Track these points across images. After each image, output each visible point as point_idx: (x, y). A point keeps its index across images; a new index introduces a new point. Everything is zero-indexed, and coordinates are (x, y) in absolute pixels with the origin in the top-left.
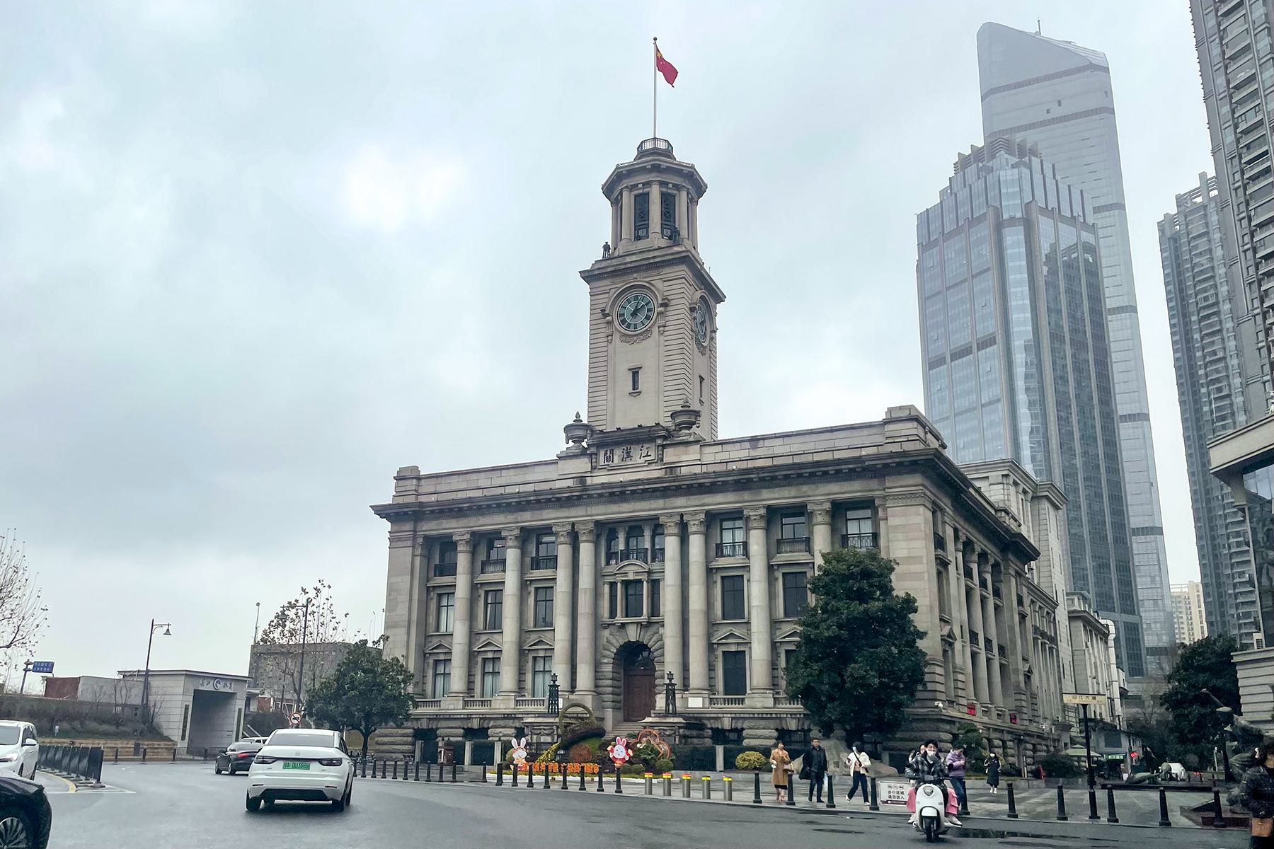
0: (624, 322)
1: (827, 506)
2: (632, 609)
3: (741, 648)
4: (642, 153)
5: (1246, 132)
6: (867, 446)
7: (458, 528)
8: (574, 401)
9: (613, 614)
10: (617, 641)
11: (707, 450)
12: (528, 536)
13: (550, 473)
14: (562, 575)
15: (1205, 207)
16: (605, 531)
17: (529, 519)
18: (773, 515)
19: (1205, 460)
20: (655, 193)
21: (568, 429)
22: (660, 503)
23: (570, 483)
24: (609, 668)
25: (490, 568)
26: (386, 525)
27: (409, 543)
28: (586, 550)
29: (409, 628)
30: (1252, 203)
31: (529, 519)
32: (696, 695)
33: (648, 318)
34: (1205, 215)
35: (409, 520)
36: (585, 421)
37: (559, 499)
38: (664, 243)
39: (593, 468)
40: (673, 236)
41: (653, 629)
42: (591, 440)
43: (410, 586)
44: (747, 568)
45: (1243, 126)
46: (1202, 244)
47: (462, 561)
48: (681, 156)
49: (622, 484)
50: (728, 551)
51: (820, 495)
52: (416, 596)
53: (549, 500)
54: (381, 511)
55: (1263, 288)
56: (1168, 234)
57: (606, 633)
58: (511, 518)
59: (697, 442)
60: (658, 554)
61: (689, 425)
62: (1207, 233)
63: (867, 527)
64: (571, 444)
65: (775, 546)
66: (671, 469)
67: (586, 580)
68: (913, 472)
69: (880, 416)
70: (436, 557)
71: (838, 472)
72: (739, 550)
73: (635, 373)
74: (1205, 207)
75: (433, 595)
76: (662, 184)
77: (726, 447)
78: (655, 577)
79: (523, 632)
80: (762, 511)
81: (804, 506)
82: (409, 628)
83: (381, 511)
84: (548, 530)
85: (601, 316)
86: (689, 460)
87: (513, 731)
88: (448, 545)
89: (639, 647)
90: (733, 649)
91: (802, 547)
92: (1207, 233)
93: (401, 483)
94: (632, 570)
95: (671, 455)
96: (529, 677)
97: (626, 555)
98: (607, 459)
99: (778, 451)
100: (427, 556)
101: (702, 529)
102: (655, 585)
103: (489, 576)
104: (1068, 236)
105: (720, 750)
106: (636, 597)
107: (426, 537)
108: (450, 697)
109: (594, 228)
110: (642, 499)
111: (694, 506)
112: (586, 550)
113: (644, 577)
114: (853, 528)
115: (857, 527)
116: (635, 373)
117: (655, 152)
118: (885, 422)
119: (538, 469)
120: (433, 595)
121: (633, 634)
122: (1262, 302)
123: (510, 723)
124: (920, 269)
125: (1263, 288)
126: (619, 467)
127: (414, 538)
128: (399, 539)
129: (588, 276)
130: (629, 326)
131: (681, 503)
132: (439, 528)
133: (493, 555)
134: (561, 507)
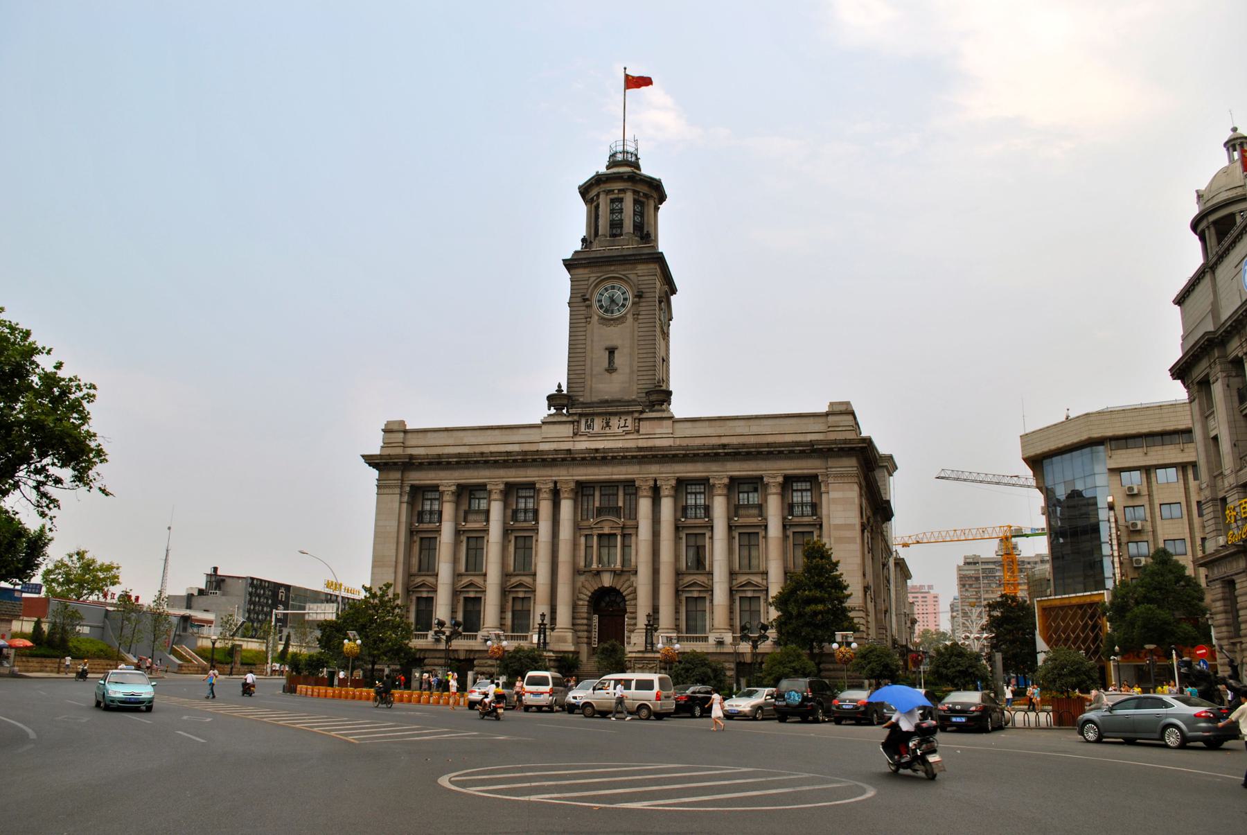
3: (430, 595)
4: (613, 163)
6: (814, 433)
7: (448, 481)
8: (557, 376)
10: (591, 586)
11: (677, 425)
12: (510, 490)
13: (534, 435)
16: (582, 490)
18: (735, 484)
20: (624, 199)
26: (375, 473)
27: (398, 491)
28: (566, 506)
35: (397, 470)
37: (544, 460)
39: (575, 434)
41: (624, 578)
44: (486, 531)
48: (647, 170)
50: (427, 518)
51: (773, 471)
52: (402, 539)
54: (371, 460)
57: (582, 578)
60: (633, 514)
64: (553, 411)
65: (734, 510)
67: (566, 532)
69: (825, 409)
72: (808, 510)
73: (611, 351)
75: (464, 538)
76: (635, 192)
79: (505, 575)
81: (707, 479)
83: (371, 460)
86: (657, 436)
89: (612, 591)
91: (755, 512)
95: (645, 427)
98: (588, 427)
107: (412, 486)
109: (571, 227)
110: (621, 464)
111: (667, 474)
112: (566, 506)
113: (618, 532)
116: (611, 351)
117: (625, 163)
118: (827, 414)
119: (522, 431)
121: (607, 580)
126: (598, 435)
127: (402, 487)
129: (569, 264)
131: (654, 470)
134: (544, 466)
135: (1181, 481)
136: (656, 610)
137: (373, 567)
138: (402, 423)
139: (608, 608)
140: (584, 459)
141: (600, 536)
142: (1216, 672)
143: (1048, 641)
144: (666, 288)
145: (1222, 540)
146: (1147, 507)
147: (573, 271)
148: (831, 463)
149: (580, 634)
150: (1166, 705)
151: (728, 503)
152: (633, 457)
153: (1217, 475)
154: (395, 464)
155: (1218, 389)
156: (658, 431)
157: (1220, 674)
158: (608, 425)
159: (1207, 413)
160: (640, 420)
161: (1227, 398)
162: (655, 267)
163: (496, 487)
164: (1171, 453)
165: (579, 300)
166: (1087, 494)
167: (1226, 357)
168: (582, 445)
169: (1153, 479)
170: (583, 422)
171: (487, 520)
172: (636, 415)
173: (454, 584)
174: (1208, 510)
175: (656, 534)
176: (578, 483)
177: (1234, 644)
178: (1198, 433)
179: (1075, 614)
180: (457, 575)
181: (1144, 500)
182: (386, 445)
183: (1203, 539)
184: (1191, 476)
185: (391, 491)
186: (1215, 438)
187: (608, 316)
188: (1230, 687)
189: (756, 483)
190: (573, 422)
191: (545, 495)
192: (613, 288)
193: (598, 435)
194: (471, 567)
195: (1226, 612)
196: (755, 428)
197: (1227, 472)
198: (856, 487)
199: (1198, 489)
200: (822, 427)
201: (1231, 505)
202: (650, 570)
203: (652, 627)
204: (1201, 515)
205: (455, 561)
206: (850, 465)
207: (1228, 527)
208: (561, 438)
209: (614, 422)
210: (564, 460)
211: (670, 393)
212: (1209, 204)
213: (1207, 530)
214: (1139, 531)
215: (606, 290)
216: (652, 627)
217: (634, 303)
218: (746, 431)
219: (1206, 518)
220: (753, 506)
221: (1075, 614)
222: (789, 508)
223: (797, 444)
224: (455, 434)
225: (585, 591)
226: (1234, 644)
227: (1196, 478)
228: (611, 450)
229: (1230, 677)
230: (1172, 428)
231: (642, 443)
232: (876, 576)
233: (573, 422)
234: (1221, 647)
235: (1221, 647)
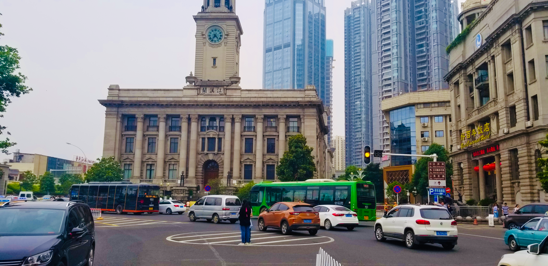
1: (285, 117)
2: (211, 148)
8: (190, 69)
9: (203, 149)
10: (205, 159)
14: (184, 133)
16: (201, 118)
17: (170, 111)
18: (267, 118)
19: (288, 104)
21: (187, 78)
24: (201, 169)
25: (150, 129)
26: (104, 108)
27: (115, 116)
28: (194, 125)
29: (115, 151)
31: (170, 111)
33: (209, 36)
36: (194, 76)
37: (184, 105)
38: (226, 10)
39: (198, 94)
40: (230, 8)
41: (219, 156)
42: (196, 82)
43: (116, 133)
49: (210, 102)
51: (282, 113)
54: (103, 103)
56: (347, 15)
57: (200, 156)
60: (222, 129)
63: (296, 124)
64: (188, 84)
65: (265, 129)
66: (230, 97)
68: (313, 108)
70: (128, 123)
72: (296, 130)
73: (215, 59)
77: (250, 92)
78: (220, 136)
82: (115, 151)
83: (103, 103)
84: (178, 116)
85: (200, 35)
86: (235, 96)
88: (132, 118)
89: (213, 161)
90: (248, 163)
93: (111, 91)
94: (212, 134)
95: (229, 93)
96: (167, 172)
97: (209, 128)
98: (204, 91)
99: (269, 96)
100: (122, 122)
101: (240, 121)
102: (220, 139)
103: (151, 132)
104: (317, 10)
106: (212, 144)
107: (123, 115)
108: (135, 179)
110: (218, 108)
111: (238, 113)
112: (194, 125)
113: (216, 137)
114: (291, 124)
115: (293, 124)
116: (215, 59)
120: (124, 138)
121: (211, 157)
124: (265, 12)
126: (208, 95)
127: (117, 115)
128: (110, 114)
131: (232, 111)
132: (127, 112)
133: (152, 124)
135: (444, 122)
136: (231, 169)
137: (104, 150)
138: (117, 86)
139: (210, 170)
141: (208, 138)
142: (453, 198)
143: (388, 183)
144: (238, 32)
145: (459, 147)
146: (430, 132)
147: (198, 22)
148: (306, 110)
149: (199, 180)
152: (223, 105)
153: (459, 121)
154: (115, 104)
155: (462, 86)
156: (234, 94)
157: (455, 199)
158: (213, 91)
159: (457, 96)
160: (227, 89)
161: (465, 91)
162: (234, 23)
163: (162, 116)
164: (441, 111)
165: (200, 34)
166: (407, 126)
167: (466, 73)
168: (201, 99)
169: (433, 121)
171: (158, 131)
172: (225, 87)
174: (454, 135)
175: (232, 138)
176: (199, 116)
177: (461, 188)
178: (452, 103)
179: (399, 174)
181: (429, 129)
183: (452, 146)
184: (448, 120)
185: (112, 117)
186: (459, 106)
188: (459, 205)
190: (197, 89)
191: (184, 120)
192: (216, 30)
193: (208, 95)
194: (150, 150)
195: (458, 175)
196: (276, 94)
197: (462, 120)
198: (315, 120)
199: (452, 125)
200: (303, 95)
201: (463, 133)
202: (229, 160)
203: (230, 177)
204: (451, 136)
205: (143, 148)
206: (313, 111)
207: (461, 142)
208: (191, 95)
209: (215, 90)
211: (239, 78)
212: (466, 9)
213: (453, 142)
214: (426, 142)
216: (230, 177)
218: (271, 96)
219: (453, 138)
220: (273, 127)
221: (399, 174)
222: (288, 129)
223: (293, 102)
225: (200, 163)
226: (461, 188)
227: (450, 121)
228: (215, 102)
229: (459, 200)
230: (442, 100)
231: (226, 99)
232: (321, 157)
233: (197, 89)
234: (456, 189)
235: (456, 189)
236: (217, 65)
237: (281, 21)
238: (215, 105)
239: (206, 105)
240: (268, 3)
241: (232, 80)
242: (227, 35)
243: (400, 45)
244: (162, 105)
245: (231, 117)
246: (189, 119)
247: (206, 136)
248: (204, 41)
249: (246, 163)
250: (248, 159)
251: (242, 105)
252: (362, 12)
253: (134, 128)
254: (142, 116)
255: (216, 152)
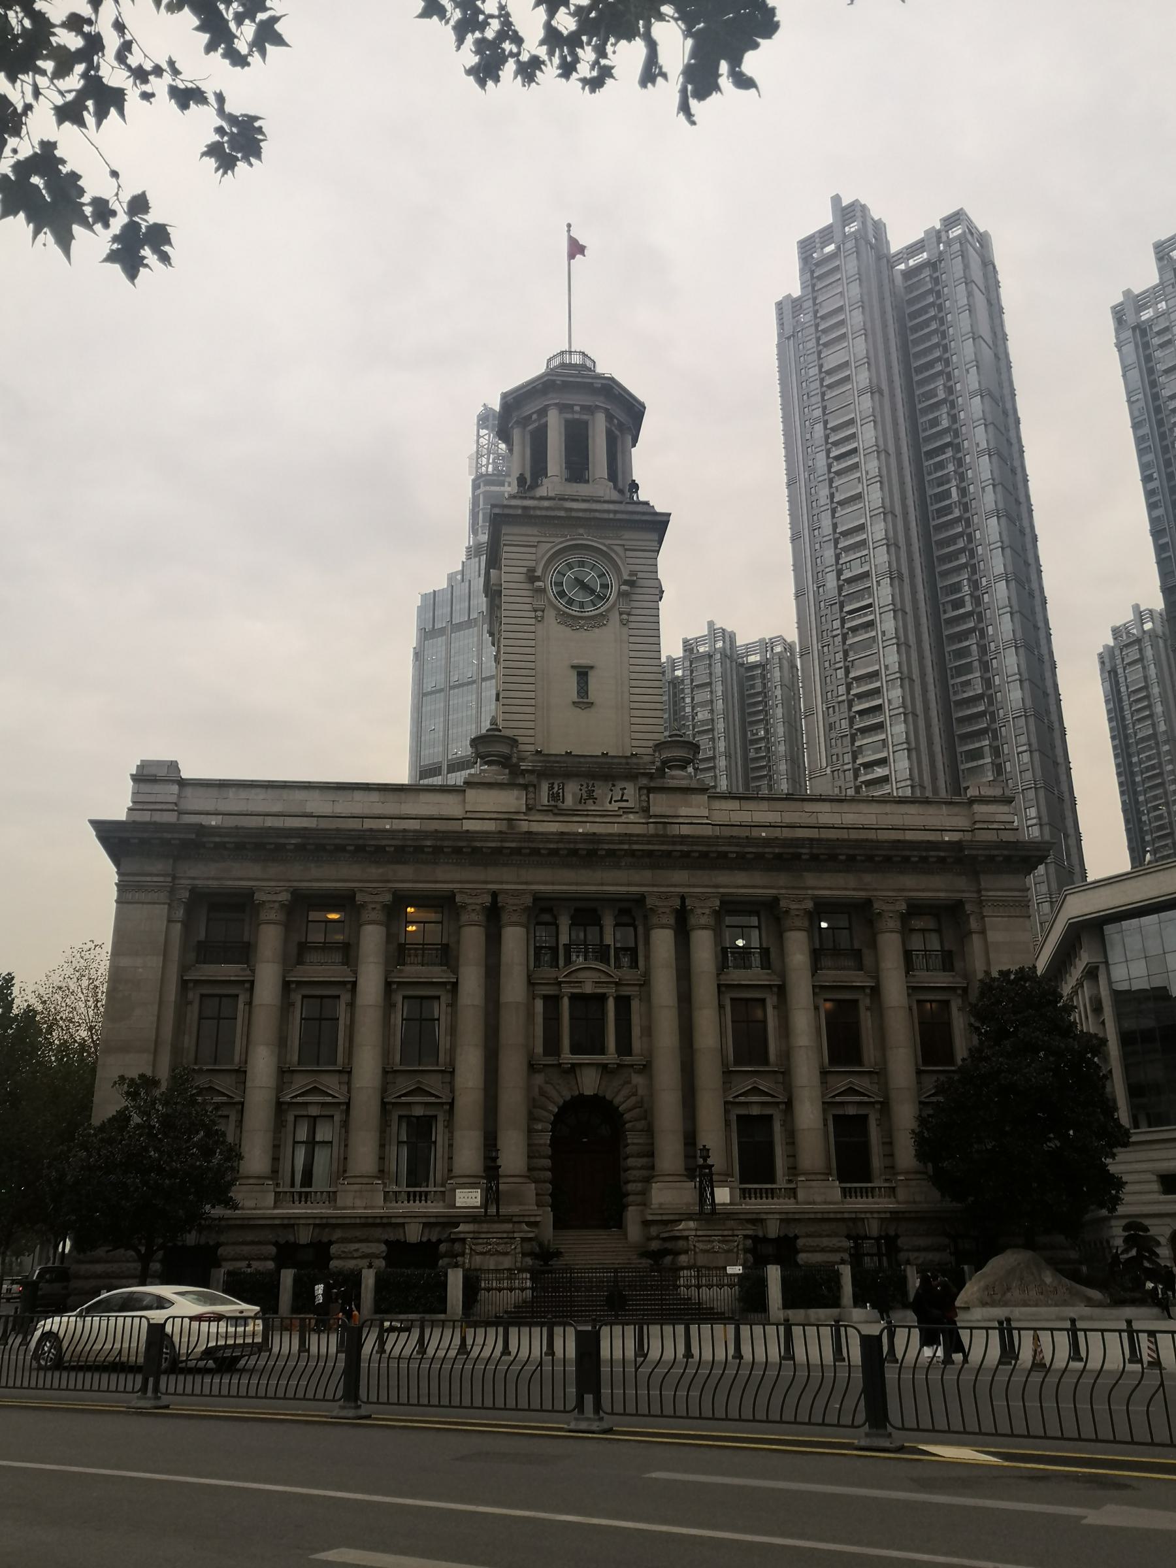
0: (562, 594)
5: (849, 581)
10: (561, 1093)
11: (717, 804)
15: (710, 656)
16: (542, 910)
22: (647, 875)
23: (490, 826)
27: (163, 896)
28: (514, 939)
29: (155, 1053)
30: (851, 653)
32: (723, 1183)
34: (710, 665)
37: (475, 850)
39: (529, 809)
45: (847, 574)
46: (703, 696)
47: (270, 940)
49: (593, 838)
53: (458, 851)
55: (857, 744)
57: (539, 1079)
58: (374, 871)
59: (703, 790)
61: (683, 764)
62: (710, 684)
66: (665, 821)
67: (514, 989)
71: (924, 859)
73: (583, 673)
74: (710, 656)
76: (563, 408)
78: (625, 991)
80: (809, 905)
81: (869, 902)
82: (155, 1053)
87: (383, 1247)
92: (710, 684)
93: (146, 788)
95: (660, 804)
98: (554, 797)
99: (824, 819)
100: (188, 926)
105: (287, 1277)
106: (588, 1021)
107: (193, 891)
112: (514, 939)
116: (583, 673)
121: (589, 1083)
122: (855, 759)
123: (378, 1233)
124: (418, 655)
125: (857, 744)
126: (573, 812)
127: (172, 891)
130: (571, 602)
131: (679, 880)
138: (174, 766)
140: (554, 852)
141: (574, 998)
150: (161, 1303)
151: (286, 940)
156: (683, 811)
158: (591, 796)
165: (521, 578)
170: (545, 787)
172: (644, 781)
173: (384, 1090)
176: (538, 898)
180: (284, 1073)
182: (138, 805)
187: (574, 611)
189: (861, 912)
192: (582, 564)
193: (573, 812)
205: (282, 1042)
210: (517, 851)
215: (570, 566)
217: (621, 594)
224: (285, 794)
233: (525, 787)
236: (592, 696)
237: (474, 682)
238: (612, 853)
239: (574, 852)
240: (429, 627)
241: (666, 754)
242: (631, 583)
243: (917, 749)
244: (380, 849)
245: (677, 903)
246: (494, 915)
247: (567, 990)
248: (540, 603)
249: (742, 1111)
250: (755, 1091)
251: (724, 855)
252: (718, 669)
253: (245, 953)
254: (285, 897)
255: (611, 1056)
